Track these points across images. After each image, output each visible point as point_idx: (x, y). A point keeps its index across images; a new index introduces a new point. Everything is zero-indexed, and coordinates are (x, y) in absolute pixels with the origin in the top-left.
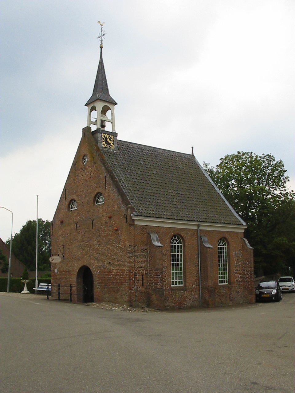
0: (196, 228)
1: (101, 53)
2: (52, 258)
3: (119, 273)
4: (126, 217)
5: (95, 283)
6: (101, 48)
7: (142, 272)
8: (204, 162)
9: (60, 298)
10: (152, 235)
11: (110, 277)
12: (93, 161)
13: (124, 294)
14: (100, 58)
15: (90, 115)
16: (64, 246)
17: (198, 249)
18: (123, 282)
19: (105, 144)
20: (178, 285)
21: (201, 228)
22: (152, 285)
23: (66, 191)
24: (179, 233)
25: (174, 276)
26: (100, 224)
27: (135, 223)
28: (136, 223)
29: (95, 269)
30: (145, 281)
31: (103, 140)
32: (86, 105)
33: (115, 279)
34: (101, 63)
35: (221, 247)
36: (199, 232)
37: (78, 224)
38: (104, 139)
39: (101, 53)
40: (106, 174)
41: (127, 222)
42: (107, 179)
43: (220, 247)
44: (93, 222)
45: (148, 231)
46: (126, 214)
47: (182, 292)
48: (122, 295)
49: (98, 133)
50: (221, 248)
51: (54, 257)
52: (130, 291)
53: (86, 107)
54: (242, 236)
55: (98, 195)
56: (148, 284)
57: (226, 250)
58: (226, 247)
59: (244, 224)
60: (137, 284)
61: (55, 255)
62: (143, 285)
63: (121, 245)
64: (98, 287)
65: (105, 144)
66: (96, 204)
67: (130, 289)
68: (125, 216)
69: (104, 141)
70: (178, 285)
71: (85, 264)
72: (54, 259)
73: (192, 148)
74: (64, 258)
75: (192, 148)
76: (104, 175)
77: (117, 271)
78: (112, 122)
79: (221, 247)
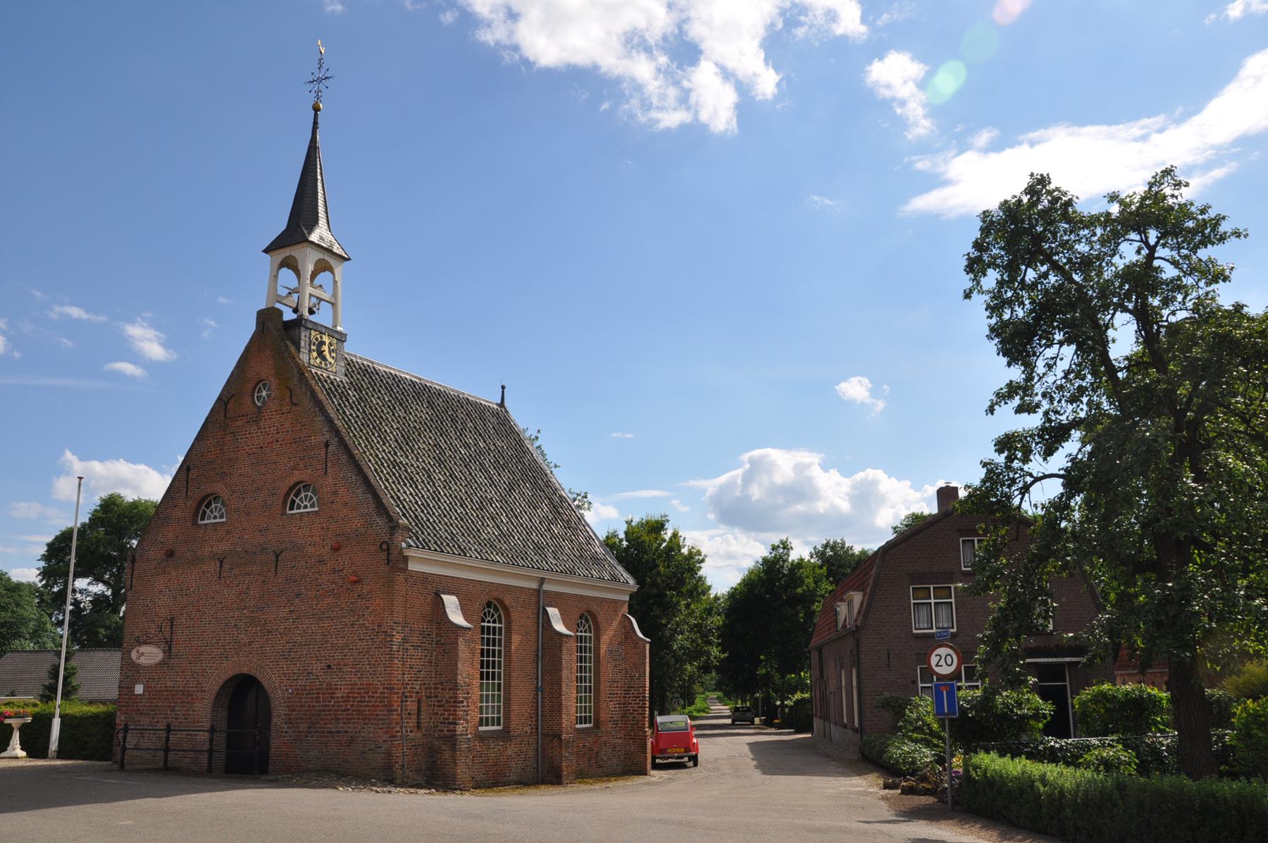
0: (534, 585)
1: (315, 123)
2: (138, 651)
3: (358, 693)
4: (388, 549)
5: (275, 720)
6: (316, 109)
7: (417, 693)
8: (991, 410)
9: (169, 765)
10: (445, 597)
11: (328, 706)
12: (288, 400)
13: (370, 750)
14: (310, 136)
15: (275, 277)
16: (172, 620)
17: (538, 636)
18: (369, 719)
19: (316, 358)
20: (490, 728)
21: (546, 587)
22: (441, 726)
23: (188, 470)
24: (501, 597)
25: (484, 704)
26: (303, 563)
27: (409, 566)
28: (412, 566)
29: (275, 681)
30: (424, 715)
31: (313, 347)
32: (266, 251)
33: (344, 710)
34: (313, 148)
35: (489, 624)
36: (541, 596)
37: (226, 561)
38: (314, 345)
39: (315, 123)
40: (327, 436)
41: (388, 564)
42: (331, 448)
43: (486, 624)
44: (280, 558)
45: (436, 588)
46: (386, 542)
47: (502, 745)
48: (364, 753)
49: (302, 329)
50: (489, 627)
51: (143, 649)
52: (391, 741)
53: (267, 257)
54: (625, 609)
55: (297, 488)
56: (430, 722)
57: (500, 634)
58: (592, 635)
59: (631, 582)
60: (407, 723)
61: (140, 643)
62: (419, 728)
63: (368, 620)
64: (286, 732)
65: (316, 358)
66: (289, 512)
67: (390, 737)
68: (385, 547)
69: (314, 351)
70: (490, 728)
71: (245, 670)
72: (143, 654)
73: (503, 387)
74: (168, 652)
75: (503, 387)
76: (323, 439)
77: (352, 689)
78: (333, 304)
79: (489, 624)
